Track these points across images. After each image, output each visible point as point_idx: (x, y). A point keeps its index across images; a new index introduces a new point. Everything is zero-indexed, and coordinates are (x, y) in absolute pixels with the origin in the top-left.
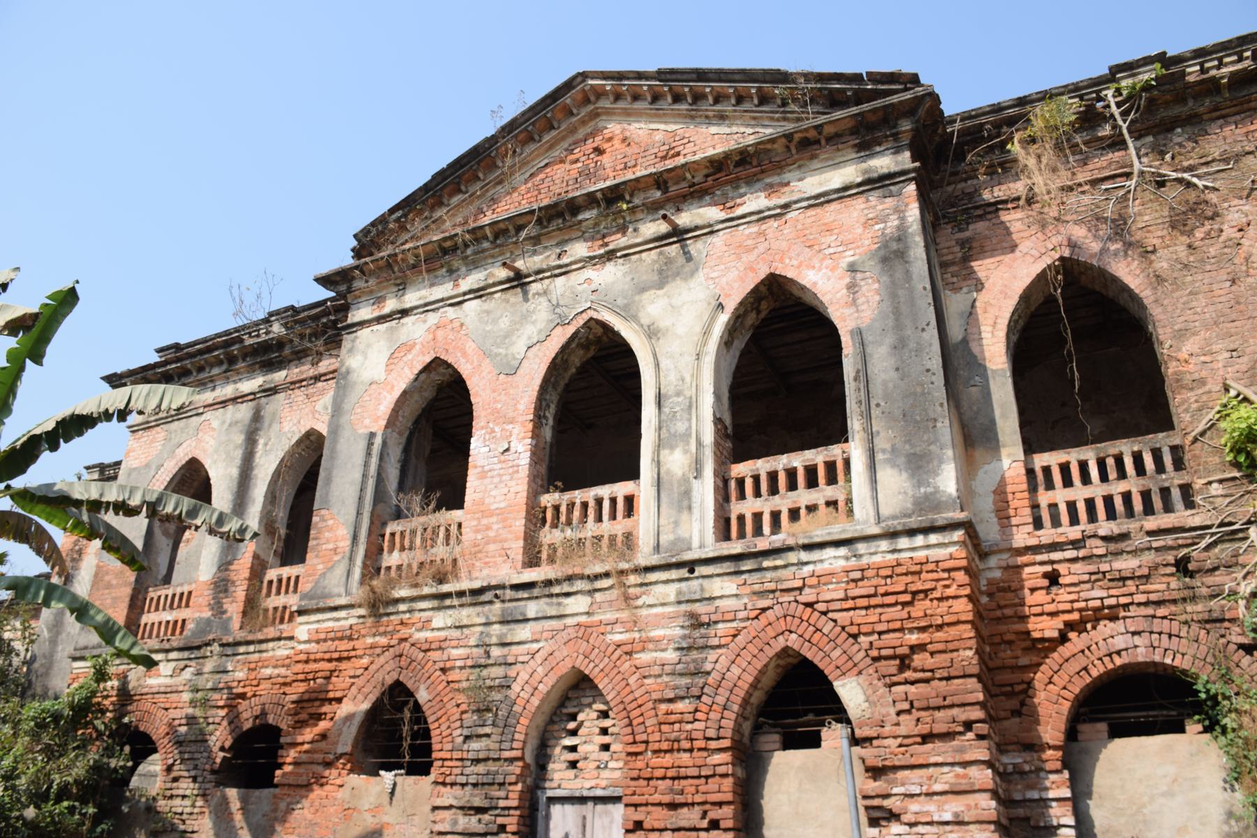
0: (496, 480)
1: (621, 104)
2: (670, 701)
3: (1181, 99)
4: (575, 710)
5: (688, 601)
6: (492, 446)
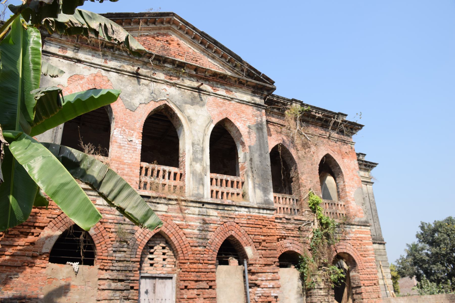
0: (127, 151)
1: (181, 32)
2: (196, 246)
3: (308, 116)
4: (153, 245)
5: (202, 215)
6: (125, 137)
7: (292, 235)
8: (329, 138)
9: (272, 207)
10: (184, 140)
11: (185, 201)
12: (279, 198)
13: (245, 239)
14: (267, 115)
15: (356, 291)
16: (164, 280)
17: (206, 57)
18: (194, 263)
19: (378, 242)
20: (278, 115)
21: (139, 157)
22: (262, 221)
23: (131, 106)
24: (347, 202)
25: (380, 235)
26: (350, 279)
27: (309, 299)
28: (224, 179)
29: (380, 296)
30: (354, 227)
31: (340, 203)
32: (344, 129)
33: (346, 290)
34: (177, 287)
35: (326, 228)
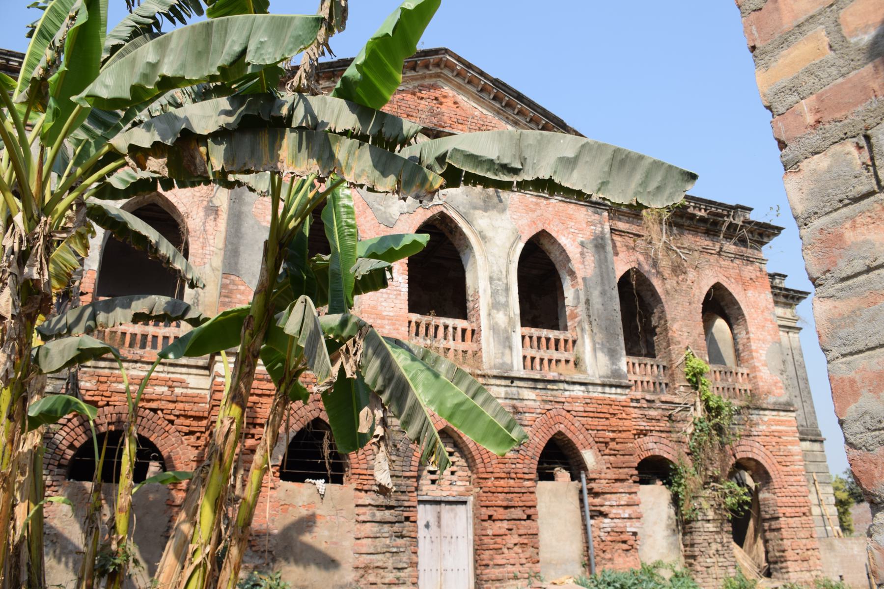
3: (682, 217)
7: (657, 429)
8: (719, 254)
9: (625, 382)
10: (476, 272)
11: (484, 376)
12: (634, 364)
13: (581, 437)
14: (610, 218)
15: (770, 525)
16: (454, 506)
17: (503, 123)
18: (502, 478)
19: (810, 437)
20: (629, 217)
21: (405, 306)
22: (608, 407)
23: (387, 219)
24: (754, 368)
25: (814, 425)
26: (759, 505)
27: (687, 537)
28: (543, 336)
29: (814, 536)
30: (767, 412)
31: (740, 370)
32: (748, 236)
33: (751, 523)
34: (476, 516)
35: (716, 416)
